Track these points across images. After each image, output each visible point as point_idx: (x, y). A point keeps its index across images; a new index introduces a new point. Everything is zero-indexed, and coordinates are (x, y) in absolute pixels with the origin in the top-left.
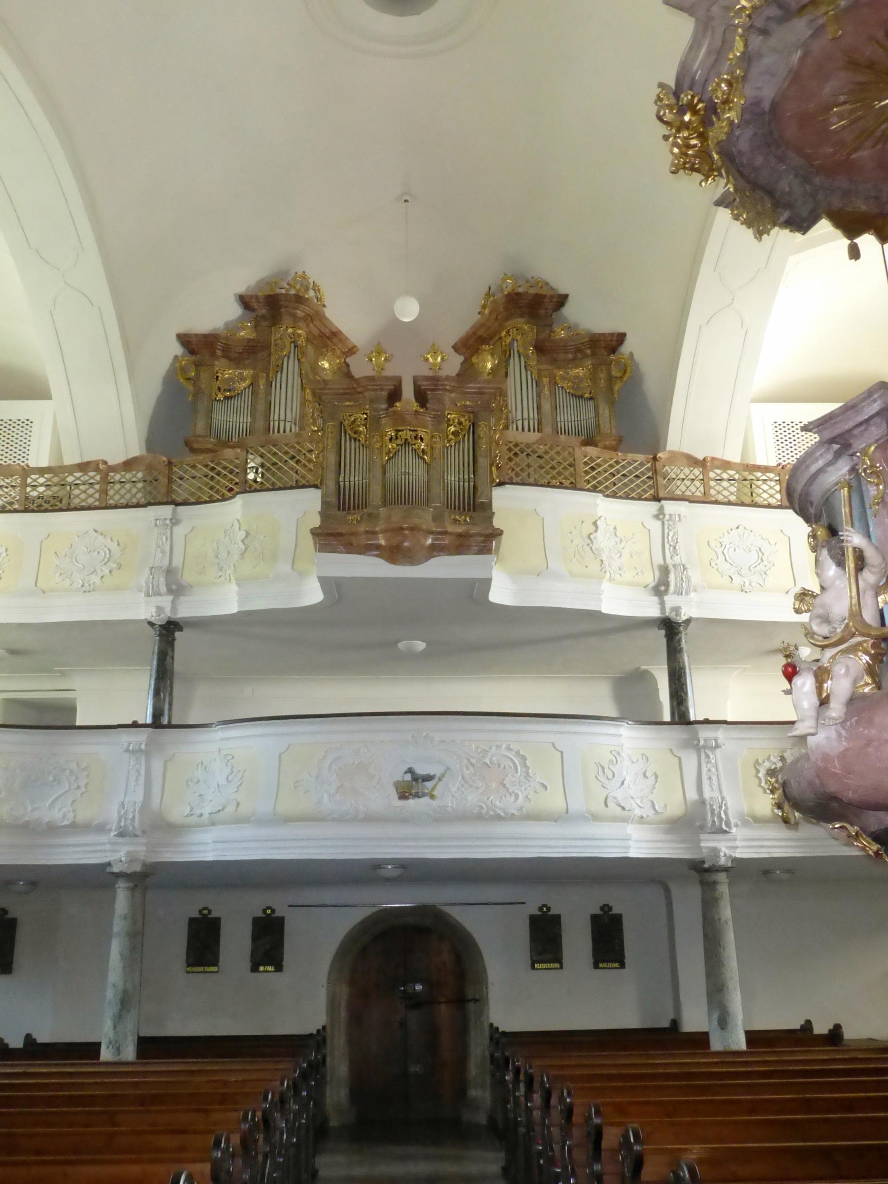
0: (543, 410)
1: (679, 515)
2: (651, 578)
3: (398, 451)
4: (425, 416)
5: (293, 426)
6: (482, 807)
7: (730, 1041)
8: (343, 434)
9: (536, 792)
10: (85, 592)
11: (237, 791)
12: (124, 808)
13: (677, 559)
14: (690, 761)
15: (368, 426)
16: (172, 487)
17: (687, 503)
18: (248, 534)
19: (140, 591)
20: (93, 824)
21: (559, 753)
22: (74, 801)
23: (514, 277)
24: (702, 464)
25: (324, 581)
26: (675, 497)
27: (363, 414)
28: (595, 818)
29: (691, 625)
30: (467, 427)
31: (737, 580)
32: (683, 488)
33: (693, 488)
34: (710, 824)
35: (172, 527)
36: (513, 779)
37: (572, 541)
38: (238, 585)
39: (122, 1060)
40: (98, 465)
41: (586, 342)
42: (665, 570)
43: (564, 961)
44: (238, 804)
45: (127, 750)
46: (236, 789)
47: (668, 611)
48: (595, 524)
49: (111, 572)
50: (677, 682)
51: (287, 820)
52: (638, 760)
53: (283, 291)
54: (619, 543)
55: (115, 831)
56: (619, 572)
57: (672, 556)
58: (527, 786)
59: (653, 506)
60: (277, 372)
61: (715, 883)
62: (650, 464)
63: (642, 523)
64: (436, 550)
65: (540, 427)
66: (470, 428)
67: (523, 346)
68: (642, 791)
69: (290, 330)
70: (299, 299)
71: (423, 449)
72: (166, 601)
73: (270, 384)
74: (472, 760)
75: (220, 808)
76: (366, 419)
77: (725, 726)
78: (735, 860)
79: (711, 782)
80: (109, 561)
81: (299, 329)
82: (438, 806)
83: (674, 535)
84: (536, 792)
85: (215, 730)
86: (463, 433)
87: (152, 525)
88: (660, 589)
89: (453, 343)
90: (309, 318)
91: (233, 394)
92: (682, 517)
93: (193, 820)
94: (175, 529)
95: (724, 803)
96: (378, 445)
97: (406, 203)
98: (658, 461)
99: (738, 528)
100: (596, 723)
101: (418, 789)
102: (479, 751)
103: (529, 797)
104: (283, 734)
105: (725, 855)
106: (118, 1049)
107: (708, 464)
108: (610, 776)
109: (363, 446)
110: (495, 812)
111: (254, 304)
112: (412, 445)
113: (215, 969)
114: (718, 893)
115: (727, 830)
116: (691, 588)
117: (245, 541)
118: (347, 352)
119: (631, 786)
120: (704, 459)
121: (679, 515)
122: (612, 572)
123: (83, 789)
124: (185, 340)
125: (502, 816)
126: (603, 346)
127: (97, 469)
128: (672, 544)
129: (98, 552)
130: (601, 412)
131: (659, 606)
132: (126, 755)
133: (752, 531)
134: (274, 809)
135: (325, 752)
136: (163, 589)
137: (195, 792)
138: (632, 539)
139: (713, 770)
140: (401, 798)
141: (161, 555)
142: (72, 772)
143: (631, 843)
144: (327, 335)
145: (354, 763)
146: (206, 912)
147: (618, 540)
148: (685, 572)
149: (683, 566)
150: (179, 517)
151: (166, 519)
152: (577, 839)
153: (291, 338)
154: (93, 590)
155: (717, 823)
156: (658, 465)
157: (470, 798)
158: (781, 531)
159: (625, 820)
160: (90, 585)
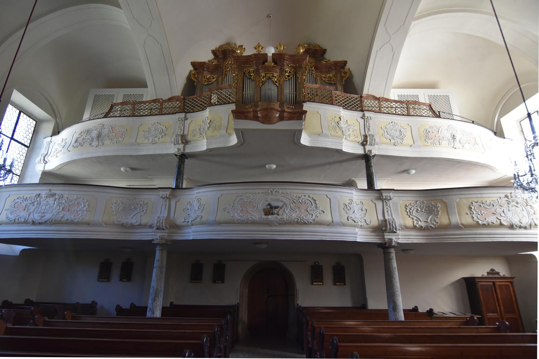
1: (370, 117)
2: (360, 139)
3: (266, 81)
4: (276, 68)
7: (398, 316)
8: (245, 77)
10: (153, 144)
12: (159, 219)
13: (370, 133)
14: (379, 204)
18: (211, 121)
19: (172, 143)
20: (148, 225)
21: (329, 199)
22: (141, 216)
28: (343, 225)
30: (293, 74)
31: (393, 141)
35: (184, 121)
38: (207, 139)
39: (154, 317)
41: (333, 64)
42: (366, 137)
43: (324, 282)
45: (162, 197)
47: (367, 151)
48: (340, 118)
49: (162, 136)
51: (220, 223)
52: (359, 204)
58: (316, 211)
59: (360, 114)
61: (390, 253)
64: (281, 118)
67: (311, 67)
72: (181, 146)
73: (222, 80)
74: (294, 201)
75: (195, 219)
76: (254, 71)
77: (393, 191)
78: (398, 243)
80: (162, 133)
82: (281, 218)
83: (368, 124)
85: (194, 190)
86: (291, 76)
88: (364, 144)
91: (210, 83)
92: (372, 118)
93: (185, 223)
94: (185, 121)
98: (362, 97)
99: (392, 122)
104: (220, 190)
105: (395, 241)
106: (153, 312)
107: (381, 99)
108: (349, 209)
109: (252, 80)
110: (304, 221)
111: (218, 54)
113: (201, 281)
114: (391, 257)
121: (370, 117)
123: (145, 212)
124: (193, 64)
126: (339, 66)
127: (159, 102)
128: (368, 127)
129: (158, 130)
130: (338, 88)
131: (363, 150)
132: (162, 199)
133: (397, 124)
134: (215, 219)
135: (236, 197)
136: (180, 142)
138: (353, 125)
139: (389, 208)
140: (265, 215)
142: (141, 205)
146: (198, 261)
147: (348, 125)
149: (373, 135)
150: (187, 117)
154: (156, 143)
157: (293, 216)
158: (408, 124)
160: (155, 141)
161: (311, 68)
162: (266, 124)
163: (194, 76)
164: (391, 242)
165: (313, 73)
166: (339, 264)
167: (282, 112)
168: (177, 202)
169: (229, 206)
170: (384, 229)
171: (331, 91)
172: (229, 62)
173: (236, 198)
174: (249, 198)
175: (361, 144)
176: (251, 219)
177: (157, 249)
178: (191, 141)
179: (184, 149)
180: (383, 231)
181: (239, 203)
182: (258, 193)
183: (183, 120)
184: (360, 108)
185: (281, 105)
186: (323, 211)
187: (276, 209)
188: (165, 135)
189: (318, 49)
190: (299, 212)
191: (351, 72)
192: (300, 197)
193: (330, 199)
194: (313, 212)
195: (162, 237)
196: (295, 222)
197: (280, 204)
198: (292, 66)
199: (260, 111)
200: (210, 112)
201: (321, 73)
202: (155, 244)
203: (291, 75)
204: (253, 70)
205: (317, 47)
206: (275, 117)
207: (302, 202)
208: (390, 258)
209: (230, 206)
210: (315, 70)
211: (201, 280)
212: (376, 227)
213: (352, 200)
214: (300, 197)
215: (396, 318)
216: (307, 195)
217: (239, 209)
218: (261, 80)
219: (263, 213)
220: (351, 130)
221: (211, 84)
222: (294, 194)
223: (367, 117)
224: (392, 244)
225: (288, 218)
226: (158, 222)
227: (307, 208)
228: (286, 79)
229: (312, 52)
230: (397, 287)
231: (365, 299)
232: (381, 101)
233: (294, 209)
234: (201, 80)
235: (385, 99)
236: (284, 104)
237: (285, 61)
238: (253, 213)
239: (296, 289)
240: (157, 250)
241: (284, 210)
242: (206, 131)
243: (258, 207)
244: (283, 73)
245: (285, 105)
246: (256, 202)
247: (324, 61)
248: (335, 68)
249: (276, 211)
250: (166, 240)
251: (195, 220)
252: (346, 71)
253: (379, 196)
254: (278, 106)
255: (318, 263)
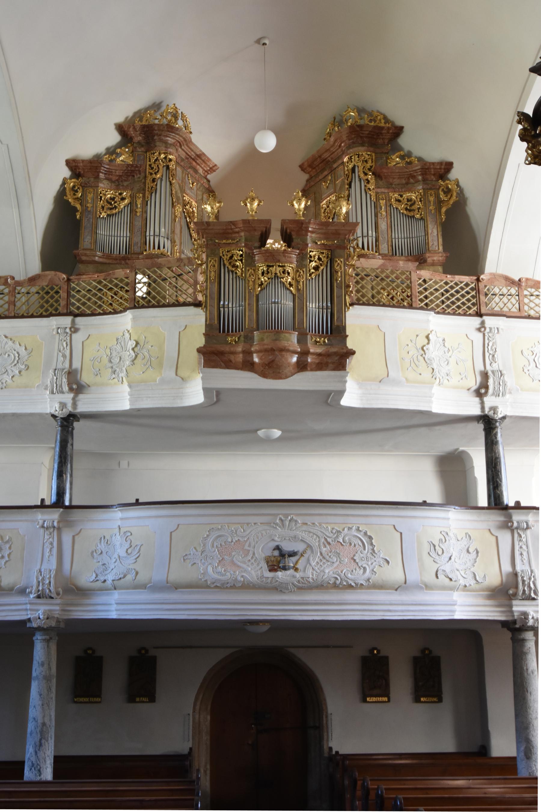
0: (380, 228)
1: (498, 329)
2: (474, 382)
3: (269, 283)
5: (166, 239)
6: (337, 578)
7: (534, 769)
9: (380, 566)
11: (135, 562)
12: (41, 575)
13: (495, 366)
14: (505, 537)
15: (243, 261)
16: (70, 300)
17: (505, 318)
18: (137, 343)
19: (46, 389)
21: (399, 534)
23: (360, 111)
24: (518, 284)
25: (206, 390)
26: (495, 313)
27: (239, 251)
28: (428, 587)
29: (507, 420)
30: (325, 263)
32: (501, 305)
33: (509, 305)
34: (521, 593)
35: (71, 335)
36: (362, 555)
37: (408, 353)
38: (130, 386)
39: (42, 780)
40: (7, 280)
42: (485, 376)
43: (391, 695)
44: (137, 573)
45: (43, 527)
46: (135, 561)
48: (427, 337)
49: (20, 372)
50: (493, 469)
51: (176, 587)
52: (462, 539)
53: (157, 122)
54: (447, 353)
55: (35, 594)
56: (447, 377)
57: (492, 363)
58: (373, 561)
59: (476, 321)
60: (152, 193)
61: (524, 640)
62: (474, 284)
63: (467, 335)
64: (301, 366)
65: (377, 243)
66: (327, 263)
67: (364, 172)
68: (465, 564)
69: (163, 156)
70: (170, 128)
71: (290, 282)
72: (68, 398)
74: (329, 540)
76: (241, 256)
79: (522, 557)
80: (18, 362)
81: (170, 154)
83: (493, 345)
84: (380, 566)
86: (322, 268)
87: (54, 333)
89: (299, 163)
90: (178, 144)
91: (114, 211)
93: (99, 584)
94: (74, 336)
95: (533, 575)
96: (253, 278)
97: (265, 46)
98: (480, 281)
100: (430, 509)
101: (285, 563)
102: (334, 532)
103: (374, 570)
105: (533, 618)
106: (39, 771)
108: (440, 553)
109: (239, 278)
110: (347, 582)
111: (131, 132)
112: (281, 278)
113: (98, 699)
114: (526, 648)
115: (535, 597)
116: (507, 391)
117: (136, 350)
118: (209, 170)
119: (456, 560)
120: (520, 280)
121: (498, 329)
122: (441, 378)
123: (7, 559)
124: (72, 164)
125: (353, 586)
126: (433, 173)
128: (491, 352)
129: (9, 355)
130: (430, 231)
132: (42, 530)
136: (66, 388)
137: (99, 562)
138: (457, 348)
139: (524, 547)
140: (270, 571)
141: (62, 358)
143: (456, 608)
144: (193, 157)
145: (232, 541)
147: (446, 349)
148: (502, 378)
149: (501, 372)
150: (77, 326)
151: (66, 328)
152: (412, 605)
153: (163, 162)
155: (527, 592)
156: (481, 285)
157: (327, 571)
159: (452, 589)
161: (366, 174)
162: (270, 378)
163: (74, 195)
164: (525, 618)
165: (369, 189)
166: (427, 652)
167: (304, 354)
168: (76, 537)
169: (194, 550)
170: (511, 592)
171: (408, 273)
172: (160, 154)
173: (208, 533)
174: (236, 533)
175: (474, 394)
176: (242, 579)
177: (37, 639)
178: (89, 386)
179: (75, 404)
180: (510, 597)
181: (215, 544)
182: (255, 524)
183: (67, 333)
184: (475, 308)
185: (302, 340)
186: (386, 560)
187: (291, 558)
188: (28, 368)
189: (382, 125)
190: (338, 562)
191: (461, 193)
192: (340, 531)
193: (401, 533)
194: (367, 562)
195: (48, 614)
196: (329, 585)
197: (299, 547)
198: (323, 244)
199: (257, 352)
200: (134, 319)
201: (388, 188)
202: (33, 628)
203: (321, 265)
204: (241, 253)
205: (380, 120)
206: (289, 364)
207: (344, 542)
208: (524, 651)
209: (197, 551)
210: (376, 180)
211: (99, 696)
212: (496, 587)
213: (447, 534)
214: (339, 532)
215: (530, 771)
216: (354, 528)
217: (215, 557)
218: (259, 279)
219: (266, 566)
220: (452, 361)
221: (116, 214)
222: (327, 525)
223: (491, 329)
224: (527, 623)
225: (317, 576)
226: (39, 582)
227: (354, 556)
228: (310, 275)
229: (367, 132)
230: (535, 711)
231: (486, 734)
232: (523, 288)
233: (327, 557)
234: (93, 207)
235: (533, 283)
236: (307, 334)
237: (309, 234)
238: (245, 566)
239: (327, 712)
240: (36, 641)
241: (308, 560)
242: (128, 369)
243: (254, 554)
244: (304, 263)
245: (309, 337)
246: (250, 542)
247: (396, 154)
248: (423, 178)
249: (291, 561)
250: (58, 621)
251: (122, 580)
252: (450, 186)
253: (505, 521)
254: (295, 340)
255: (378, 651)
